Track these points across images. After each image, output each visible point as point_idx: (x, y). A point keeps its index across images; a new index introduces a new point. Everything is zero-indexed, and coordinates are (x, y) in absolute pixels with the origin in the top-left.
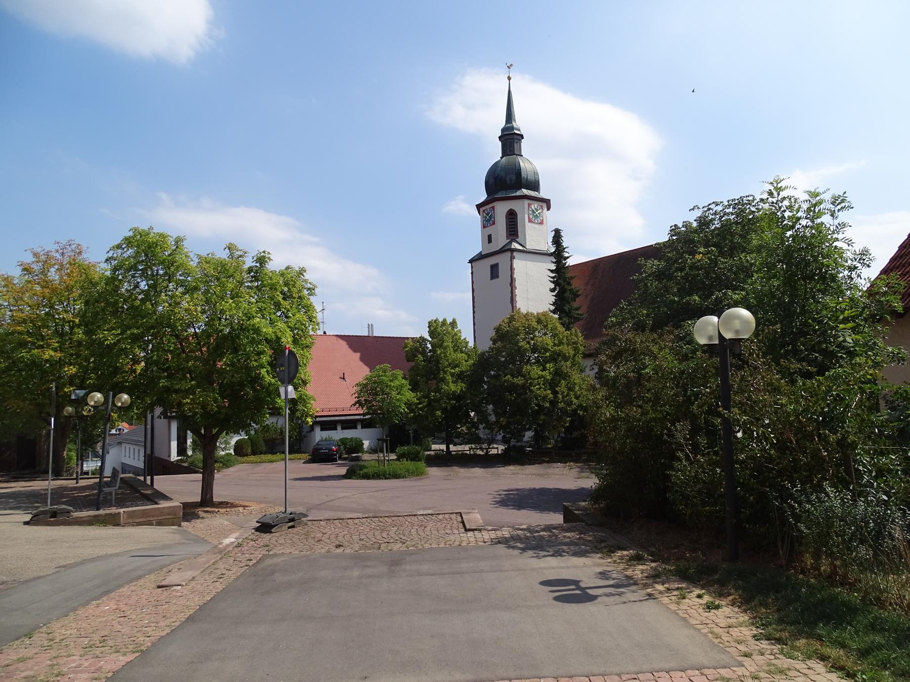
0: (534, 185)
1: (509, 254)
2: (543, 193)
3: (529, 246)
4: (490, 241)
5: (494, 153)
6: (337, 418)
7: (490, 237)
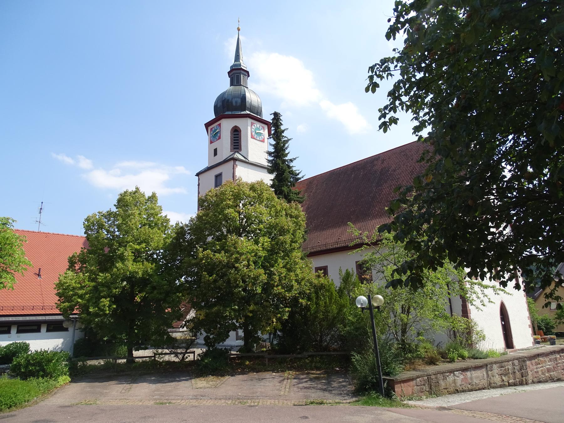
1: (232, 162)
3: (251, 159)
4: (215, 154)
5: (224, 85)
6: (11, 319)
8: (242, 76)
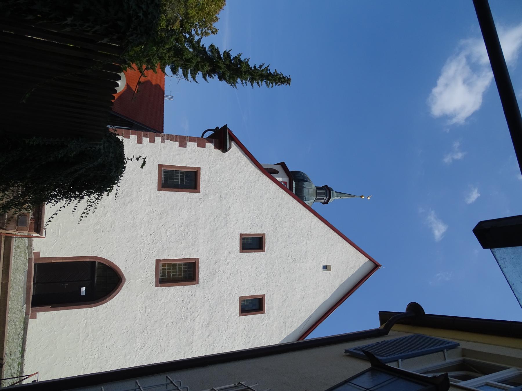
8: (324, 192)
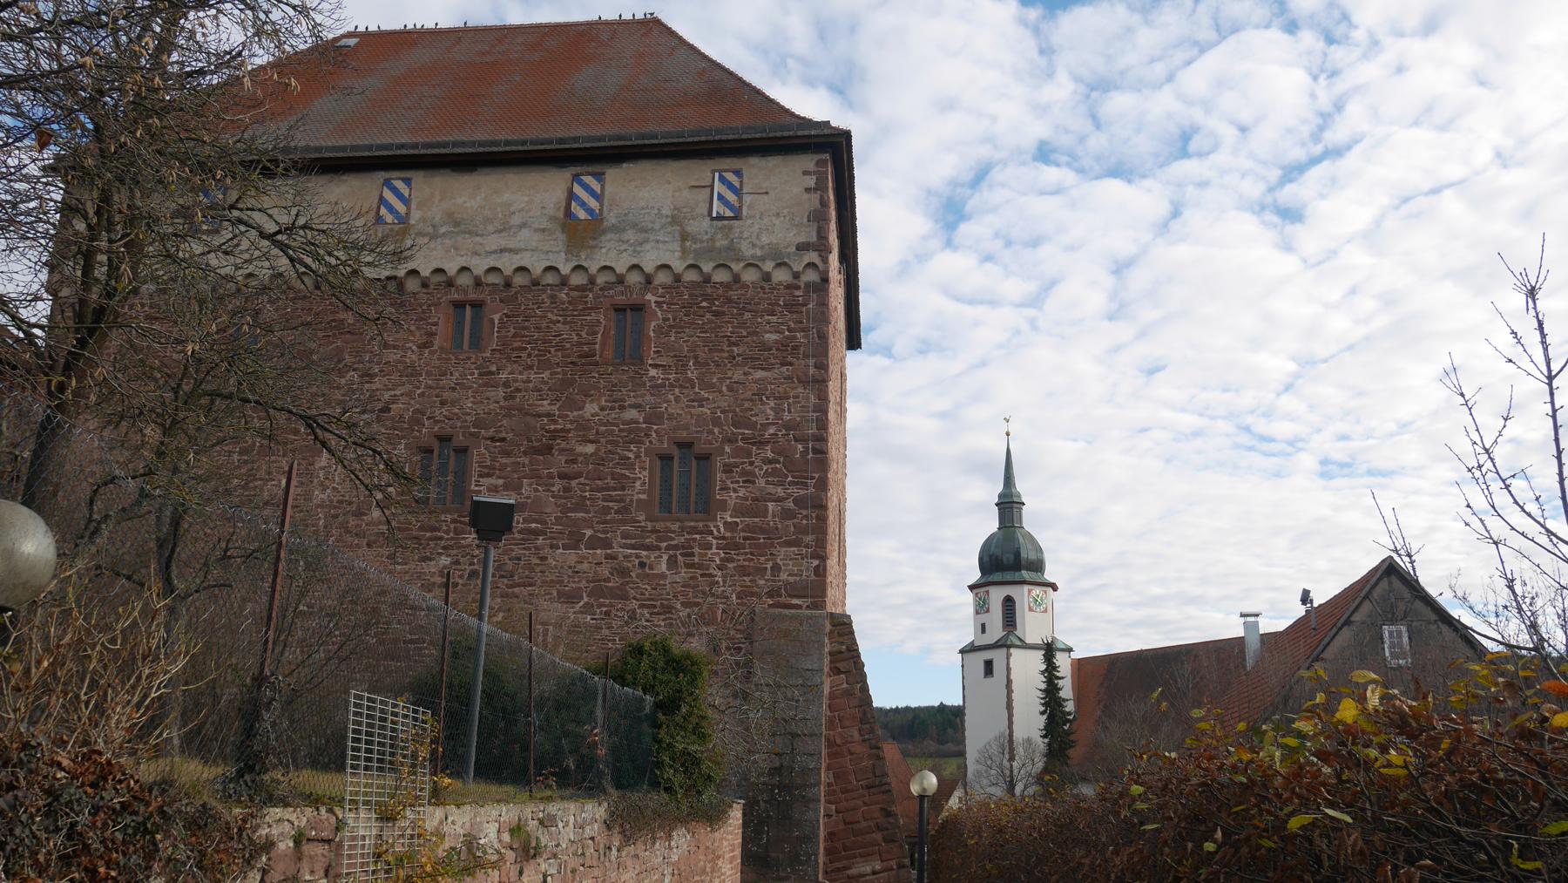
0: (1038, 566)
2: (1049, 575)
4: (983, 631)
7: (983, 626)
